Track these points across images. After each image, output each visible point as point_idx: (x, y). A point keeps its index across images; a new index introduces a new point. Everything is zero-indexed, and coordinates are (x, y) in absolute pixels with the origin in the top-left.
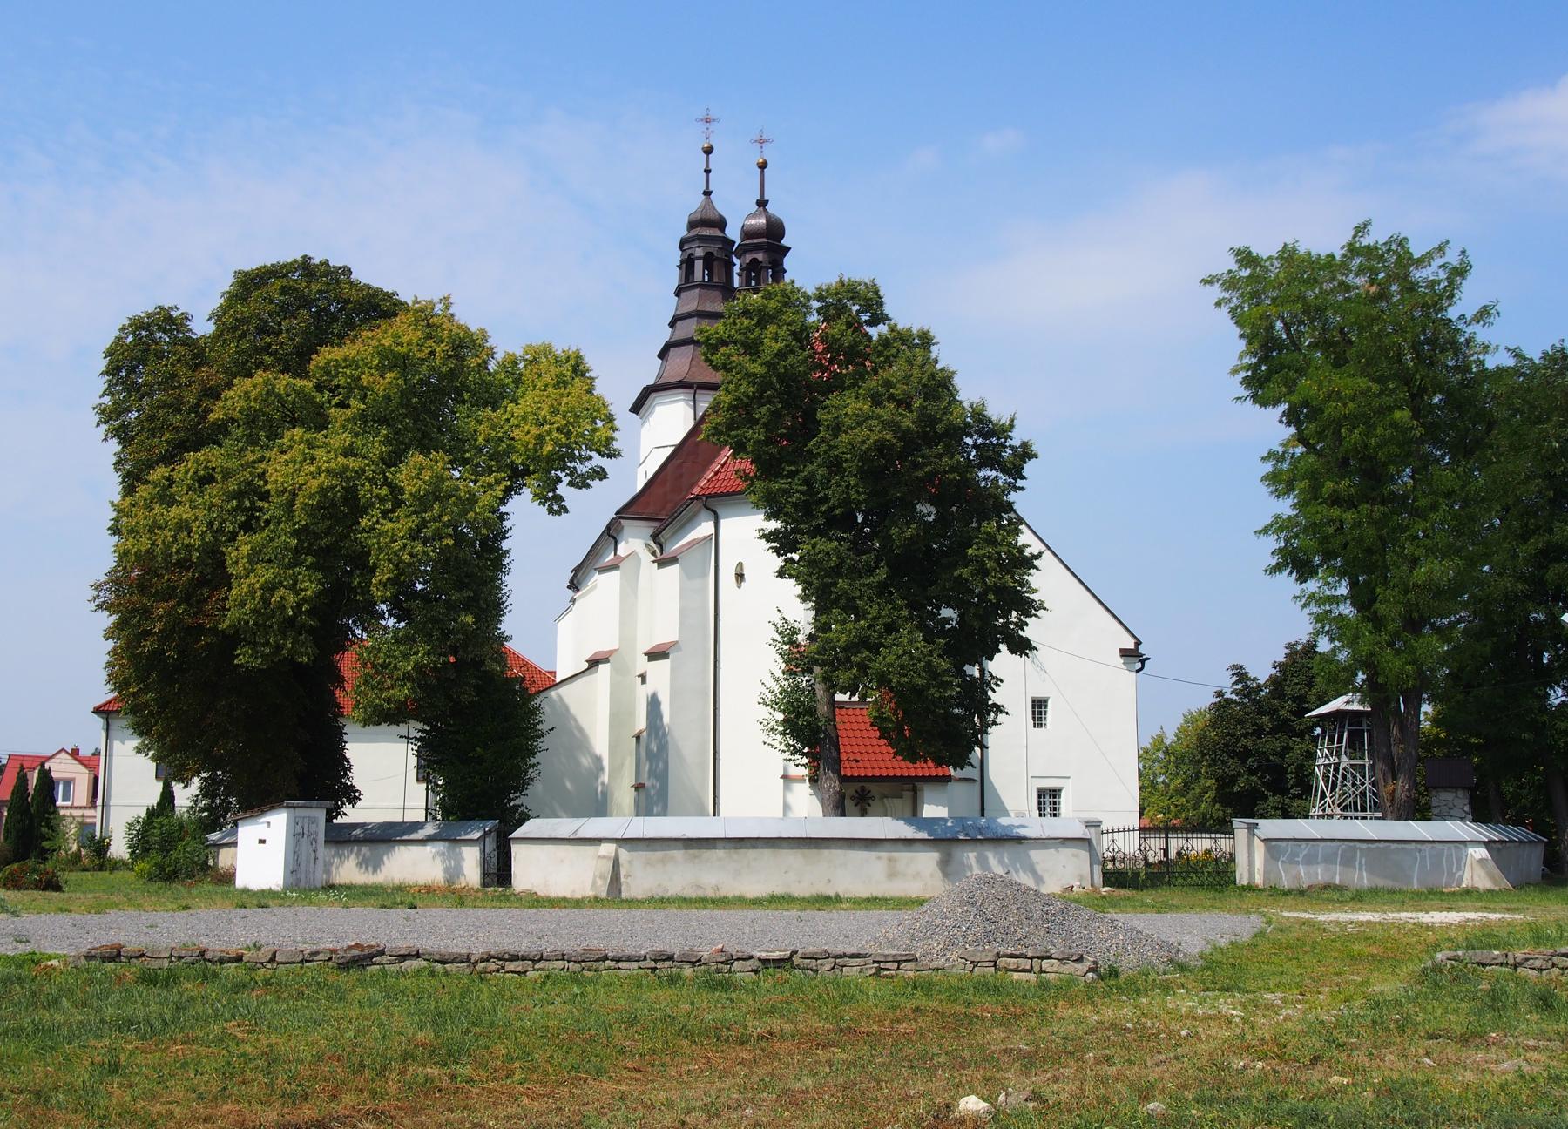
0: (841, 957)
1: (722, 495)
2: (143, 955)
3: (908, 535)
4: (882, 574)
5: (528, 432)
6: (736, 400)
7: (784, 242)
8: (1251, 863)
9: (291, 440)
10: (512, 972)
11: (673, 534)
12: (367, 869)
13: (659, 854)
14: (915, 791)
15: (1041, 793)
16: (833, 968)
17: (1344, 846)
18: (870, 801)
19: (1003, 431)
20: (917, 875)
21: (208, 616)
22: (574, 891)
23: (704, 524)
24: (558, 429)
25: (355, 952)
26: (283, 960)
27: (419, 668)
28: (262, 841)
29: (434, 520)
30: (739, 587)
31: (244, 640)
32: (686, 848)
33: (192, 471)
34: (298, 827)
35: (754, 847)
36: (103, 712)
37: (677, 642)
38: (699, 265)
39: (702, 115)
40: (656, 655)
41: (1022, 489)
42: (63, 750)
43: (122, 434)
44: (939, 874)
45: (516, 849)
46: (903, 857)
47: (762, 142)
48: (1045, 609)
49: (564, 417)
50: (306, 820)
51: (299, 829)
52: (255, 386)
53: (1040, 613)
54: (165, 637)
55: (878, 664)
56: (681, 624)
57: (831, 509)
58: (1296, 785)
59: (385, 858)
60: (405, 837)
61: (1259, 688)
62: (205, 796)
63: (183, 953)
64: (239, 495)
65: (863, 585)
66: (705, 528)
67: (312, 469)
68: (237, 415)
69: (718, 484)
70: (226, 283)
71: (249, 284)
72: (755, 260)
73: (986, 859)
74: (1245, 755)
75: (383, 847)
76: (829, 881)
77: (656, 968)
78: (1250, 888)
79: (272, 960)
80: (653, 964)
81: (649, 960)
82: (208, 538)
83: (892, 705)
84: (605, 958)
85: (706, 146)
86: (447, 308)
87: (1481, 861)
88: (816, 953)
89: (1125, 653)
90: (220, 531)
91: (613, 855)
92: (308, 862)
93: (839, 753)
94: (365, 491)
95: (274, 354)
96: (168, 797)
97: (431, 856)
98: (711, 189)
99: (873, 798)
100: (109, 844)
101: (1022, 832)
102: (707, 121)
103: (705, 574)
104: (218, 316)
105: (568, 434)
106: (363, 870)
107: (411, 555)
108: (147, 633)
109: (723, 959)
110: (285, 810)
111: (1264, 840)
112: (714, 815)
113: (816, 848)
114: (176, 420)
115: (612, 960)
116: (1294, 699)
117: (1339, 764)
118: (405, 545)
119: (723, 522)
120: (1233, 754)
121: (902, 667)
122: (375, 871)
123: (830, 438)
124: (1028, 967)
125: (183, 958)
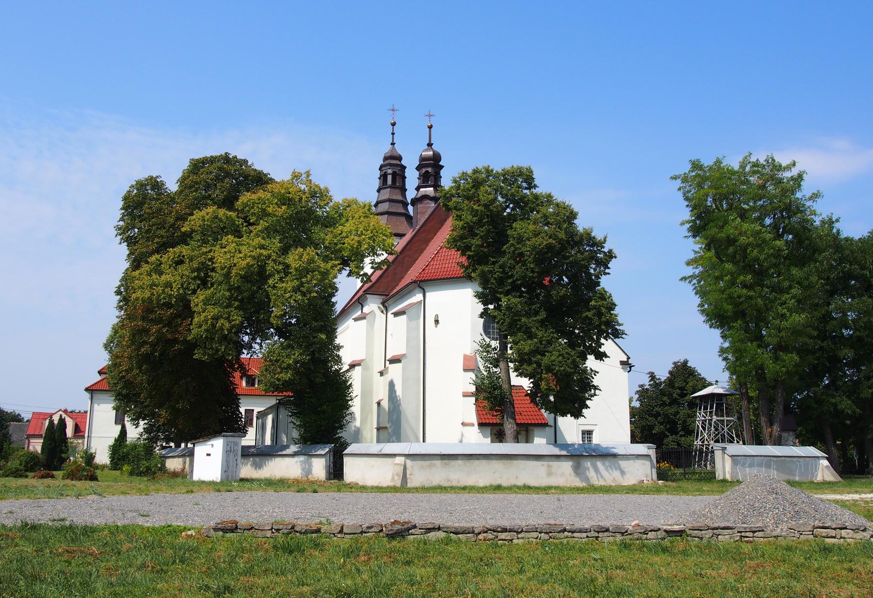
0: (716, 529)
1: (428, 280)
2: (252, 528)
3: (561, 294)
4: (543, 315)
5: (353, 240)
6: (465, 223)
9: (227, 241)
10: (502, 540)
11: (398, 299)
13: (427, 463)
14: (527, 431)
15: (583, 432)
16: (712, 536)
19: (601, 244)
21: (180, 333)
22: (380, 482)
23: (417, 295)
24: (370, 238)
25: (398, 527)
26: (349, 532)
27: (296, 362)
28: (209, 455)
30: (436, 327)
31: (199, 346)
33: (172, 257)
34: (229, 447)
36: (90, 390)
37: (405, 354)
38: (390, 178)
40: (395, 360)
41: (609, 274)
42: (60, 410)
43: (130, 241)
44: (573, 474)
45: (346, 460)
46: (555, 464)
47: (430, 116)
48: (626, 334)
49: (372, 232)
50: (233, 443)
51: (229, 449)
52: (207, 214)
53: (624, 336)
54: (153, 345)
55: (545, 361)
56: (407, 345)
57: (514, 282)
58: (682, 430)
60: (280, 453)
61: (661, 383)
62: (146, 432)
63: (281, 527)
64: (198, 270)
65: (533, 321)
66: (419, 297)
67: (241, 255)
68: (197, 228)
69: (425, 275)
70: (185, 165)
71: (197, 166)
72: (427, 171)
73: (596, 465)
74: (657, 415)
76: (517, 477)
77: (599, 537)
78: (724, 481)
79: (341, 532)
80: (596, 535)
81: (592, 532)
82: (181, 291)
83: (555, 383)
84: (565, 530)
86: (308, 176)
87: (827, 466)
88: (701, 527)
89: (622, 363)
90: (188, 288)
92: (233, 466)
93: (514, 408)
94: (270, 267)
95: (212, 200)
96: (123, 433)
100: (95, 457)
101: (615, 451)
102: (393, 110)
103: (419, 318)
104: (182, 181)
105: (374, 241)
107: (295, 300)
108: (145, 343)
109: (643, 531)
111: (730, 456)
112: (424, 441)
113: (510, 460)
114: (162, 232)
115: (569, 532)
117: (712, 420)
118: (291, 296)
119: (428, 294)
120: (651, 415)
121: (560, 362)
123: (516, 244)
124: (834, 535)
125: (280, 530)
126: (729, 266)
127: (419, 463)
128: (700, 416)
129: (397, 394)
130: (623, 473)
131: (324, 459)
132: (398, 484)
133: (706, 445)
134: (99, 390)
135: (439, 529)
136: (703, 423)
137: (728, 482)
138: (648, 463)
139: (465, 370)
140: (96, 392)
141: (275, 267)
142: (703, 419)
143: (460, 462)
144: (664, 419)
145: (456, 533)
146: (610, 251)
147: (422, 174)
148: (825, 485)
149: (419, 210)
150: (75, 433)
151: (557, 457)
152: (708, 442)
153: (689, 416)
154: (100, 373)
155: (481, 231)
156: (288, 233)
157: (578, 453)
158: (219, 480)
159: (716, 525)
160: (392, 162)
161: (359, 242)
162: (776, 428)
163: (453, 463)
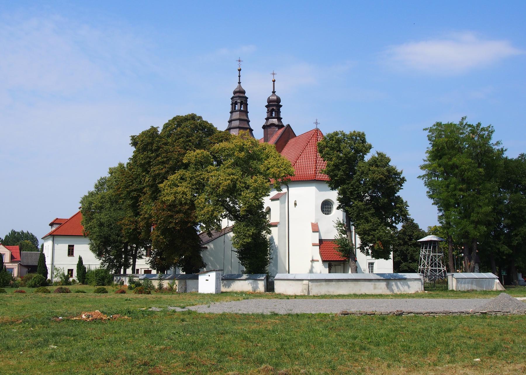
8: (452, 284)
12: (226, 287)
13: (319, 283)
15: (369, 264)
17: (471, 279)
20: (381, 288)
24: (284, 169)
29: (260, 194)
32: (326, 282)
35: (342, 281)
41: (403, 189)
45: (275, 282)
46: (378, 283)
47: (274, 74)
59: (232, 284)
60: (239, 278)
63: (363, 313)
68: (193, 161)
75: (231, 281)
78: (453, 291)
84: (450, 313)
98: (241, 82)
99: (332, 266)
102: (239, 61)
103: (285, 202)
113: (357, 281)
116: (409, 236)
119: (290, 189)
122: (228, 287)
126: (454, 179)
127: (315, 283)
128: (423, 252)
129: (276, 244)
130: (409, 287)
133: (426, 268)
134: (58, 235)
135: (412, 313)
136: (424, 256)
137: (455, 291)
138: (420, 283)
139: (313, 232)
140: (56, 236)
142: (424, 254)
143: (334, 283)
144: (400, 253)
145: (417, 314)
146: (403, 178)
148: (498, 292)
149: (269, 133)
150: (11, 259)
151: (379, 280)
152: (428, 267)
153: (414, 251)
154: (52, 225)
155: (343, 168)
157: (388, 278)
158: (214, 293)
159: (496, 310)
161: (279, 171)
162: (472, 263)
163: (331, 283)
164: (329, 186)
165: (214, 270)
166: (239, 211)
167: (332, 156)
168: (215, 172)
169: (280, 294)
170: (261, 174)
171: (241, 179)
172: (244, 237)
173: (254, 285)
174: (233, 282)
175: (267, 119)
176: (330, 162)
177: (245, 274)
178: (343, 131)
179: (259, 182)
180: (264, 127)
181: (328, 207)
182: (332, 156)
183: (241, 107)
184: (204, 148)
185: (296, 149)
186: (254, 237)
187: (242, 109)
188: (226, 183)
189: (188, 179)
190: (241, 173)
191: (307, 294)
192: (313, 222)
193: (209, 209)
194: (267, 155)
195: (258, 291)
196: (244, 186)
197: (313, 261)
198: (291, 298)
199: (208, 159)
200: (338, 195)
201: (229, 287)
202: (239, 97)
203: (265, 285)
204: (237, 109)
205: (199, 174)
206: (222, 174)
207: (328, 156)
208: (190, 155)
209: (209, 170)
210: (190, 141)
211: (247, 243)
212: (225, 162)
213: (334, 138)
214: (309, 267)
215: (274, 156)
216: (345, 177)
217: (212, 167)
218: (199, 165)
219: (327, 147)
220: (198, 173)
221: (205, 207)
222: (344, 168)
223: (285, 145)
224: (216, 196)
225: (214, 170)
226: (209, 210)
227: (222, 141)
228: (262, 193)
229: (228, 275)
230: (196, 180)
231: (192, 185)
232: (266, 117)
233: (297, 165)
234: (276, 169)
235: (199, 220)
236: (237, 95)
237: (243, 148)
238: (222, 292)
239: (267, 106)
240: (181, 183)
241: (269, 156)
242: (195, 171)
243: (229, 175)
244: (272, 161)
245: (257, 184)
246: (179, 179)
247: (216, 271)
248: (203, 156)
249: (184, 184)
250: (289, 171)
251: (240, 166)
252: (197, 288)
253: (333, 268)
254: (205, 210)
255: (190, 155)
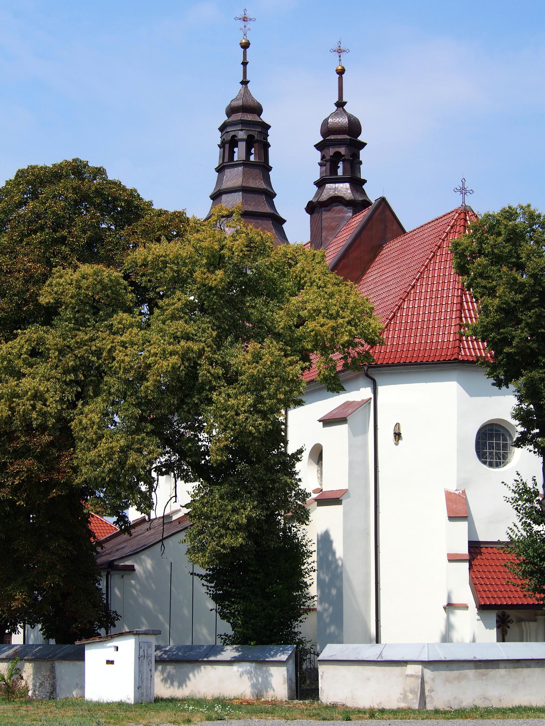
7: (361, 138)
12: (172, 684)
13: (455, 673)
18: (510, 625)
23: (362, 390)
24: (349, 323)
29: (270, 397)
30: (397, 444)
32: (477, 668)
34: (142, 650)
35: (529, 667)
39: (241, 14)
45: (322, 669)
47: (340, 51)
56: (350, 475)
59: (191, 675)
60: (212, 658)
68: (68, 300)
75: (187, 667)
85: (244, 41)
91: (420, 674)
92: (147, 679)
97: (238, 674)
99: (511, 621)
102: (245, 19)
103: (365, 431)
106: (168, 685)
110: (134, 637)
119: (380, 389)
122: (180, 685)
127: (443, 674)
131: (285, 668)
132: (416, 706)
139: (451, 518)
141: (212, 371)
143: (502, 672)
147: (328, 158)
149: (325, 224)
156: (220, 312)
158: (131, 701)
160: (246, 118)
161: (333, 329)
164: (489, 374)
165: (130, 633)
166: (207, 453)
167: (494, 283)
168: (135, 330)
169: (334, 707)
170: (278, 336)
171: (215, 353)
172: (223, 532)
173: (257, 680)
174: (193, 670)
175: (320, 184)
176: (488, 300)
177: (233, 643)
178: (529, 206)
179: (267, 359)
180: (311, 208)
181: (498, 445)
182: (494, 283)
183: (248, 154)
184: (109, 262)
185: (402, 269)
186: (253, 530)
187: (252, 158)
188: (165, 363)
189: (54, 354)
190: (215, 334)
191: (416, 706)
192: (452, 489)
193: (114, 444)
194: (300, 281)
195: (269, 696)
196: (223, 374)
197: (450, 607)
198: (360, 718)
199: (116, 293)
200: (517, 402)
201: (182, 683)
202: (244, 123)
203: (289, 679)
204: (236, 159)
205: (87, 338)
206: (155, 337)
207: (484, 282)
208: (61, 281)
209: (117, 326)
210: (63, 240)
211: (232, 548)
212: (166, 301)
213: (502, 227)
214: (441, 627)
215: (320, 283)
216: (535, 346)
217: (125, 315)
218: (87, 312)
219: (480, 253)
220: (81, 336)
221: (100, 437)
222: (531, 317)
223: (372, 260)
224: (135, 406)
225: (131, 326)
226: (112, 448)
227: (158, 240)
228: (275, 394)
229: (179, 648)
230: (76, 356)
231: (66, 372)
232: (317, 177)
233: (402, 316)
234: (322, 320)
235: (83, 479)
236: (238, 116)
237: (222, 257)
238: (158, 700)
239: (319, 147)
240: (31, 366)
241: (305, 282)
242: (74, 329)
243: (177, 339)
244: (312, 297)
245: (260, 367)
246: (25, 353)
247: (137, 634)
248: (101, 282)
249: (42, 368)
250: (365, 327)
251: (213, 313)
252: (82, 688)
253: (513, 629)
254: (103, 446)
255: (61, 281)
